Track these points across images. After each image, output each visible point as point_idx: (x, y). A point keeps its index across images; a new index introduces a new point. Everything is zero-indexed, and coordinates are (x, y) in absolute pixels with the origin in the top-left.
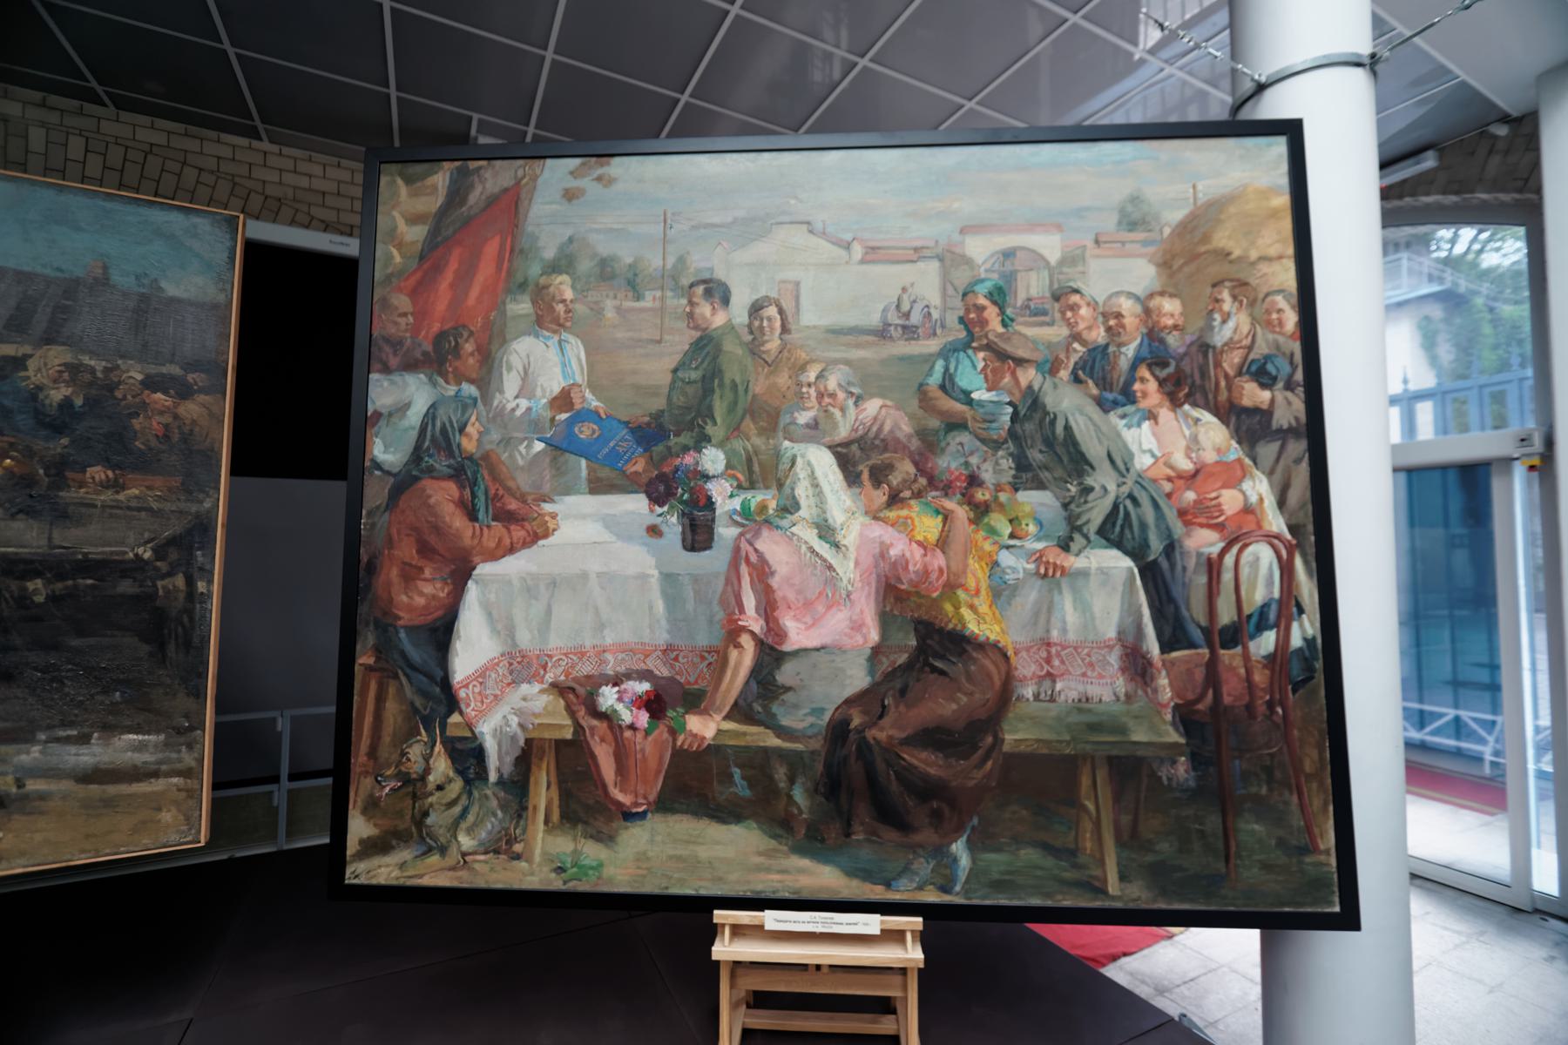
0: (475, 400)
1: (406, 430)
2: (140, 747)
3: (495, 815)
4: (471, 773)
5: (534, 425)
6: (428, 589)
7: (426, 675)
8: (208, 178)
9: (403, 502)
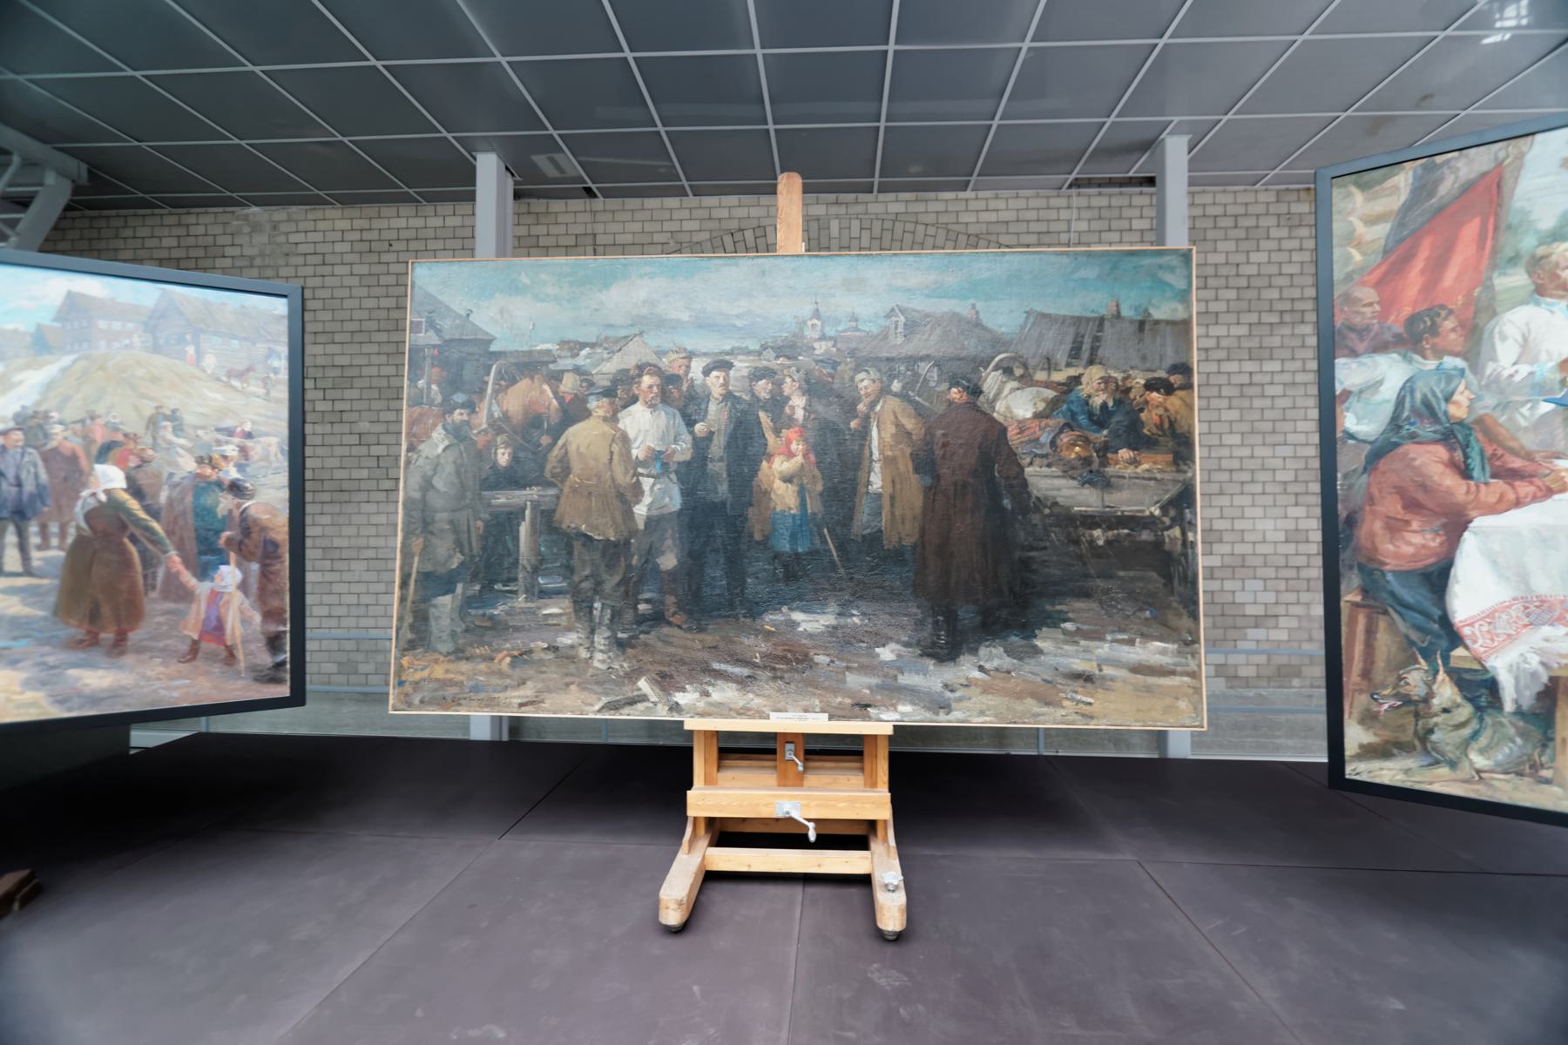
0: (1462, 372)
1: (1380, 404)
2: (1163, 652)
3: (1513, 742)
4: (1483, 701)
5: (1540, 389)
6: (1417, 539)
7: (1422, 613)
8: (931, 231)
9: (1383, 465)
